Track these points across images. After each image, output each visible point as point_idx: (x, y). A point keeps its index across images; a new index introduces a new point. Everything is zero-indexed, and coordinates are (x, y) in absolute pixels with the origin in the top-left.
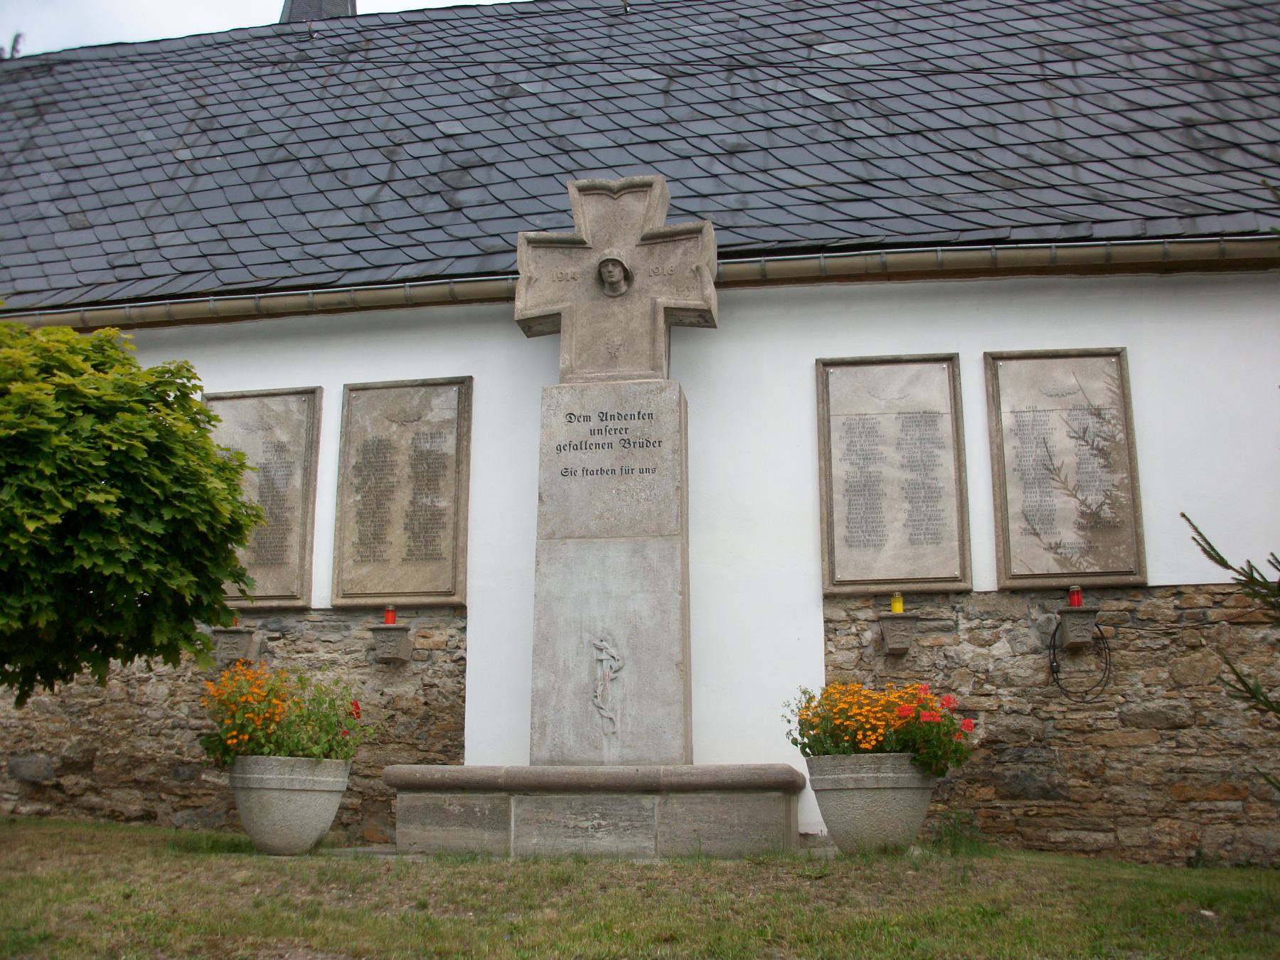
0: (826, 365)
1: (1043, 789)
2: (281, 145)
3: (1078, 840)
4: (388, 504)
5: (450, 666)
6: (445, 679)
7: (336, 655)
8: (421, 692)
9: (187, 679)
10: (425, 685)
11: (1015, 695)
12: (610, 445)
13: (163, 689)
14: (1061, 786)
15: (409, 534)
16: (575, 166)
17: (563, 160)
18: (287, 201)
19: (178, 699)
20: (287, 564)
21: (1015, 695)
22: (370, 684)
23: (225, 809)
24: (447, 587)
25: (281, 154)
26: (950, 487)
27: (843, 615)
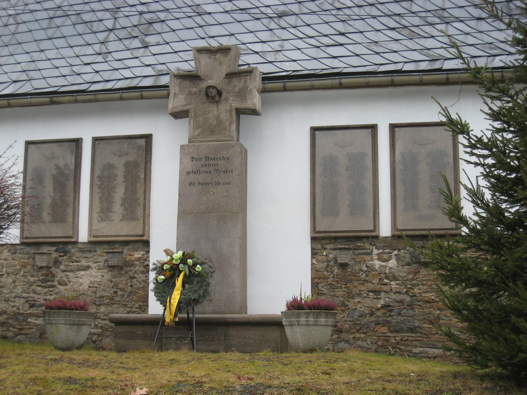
0: (314, 130)
1: (410, 328)
2: (60, 7)
3: (426, 352)
4: (113, 194)
5: (142, 269)
6: (140, 275)
7: (90, 264)
8: (129, 281)
9: (21, 275)
10: (131, 278)
11: (398, 284)
12: (210, 172)
13: (10, 280)
14: (418, 327)
15: (123, 208)
16: (203, 23)
17: (198, 19)
18: (63, 40)
19: (17, 284)
20: (67, 222)
21: (398, 284)
22: (106, 277)
23: (39, 335)
24: (140, 233)
25: (59, 13)
26: (370, 188)
27: (320, 246)
